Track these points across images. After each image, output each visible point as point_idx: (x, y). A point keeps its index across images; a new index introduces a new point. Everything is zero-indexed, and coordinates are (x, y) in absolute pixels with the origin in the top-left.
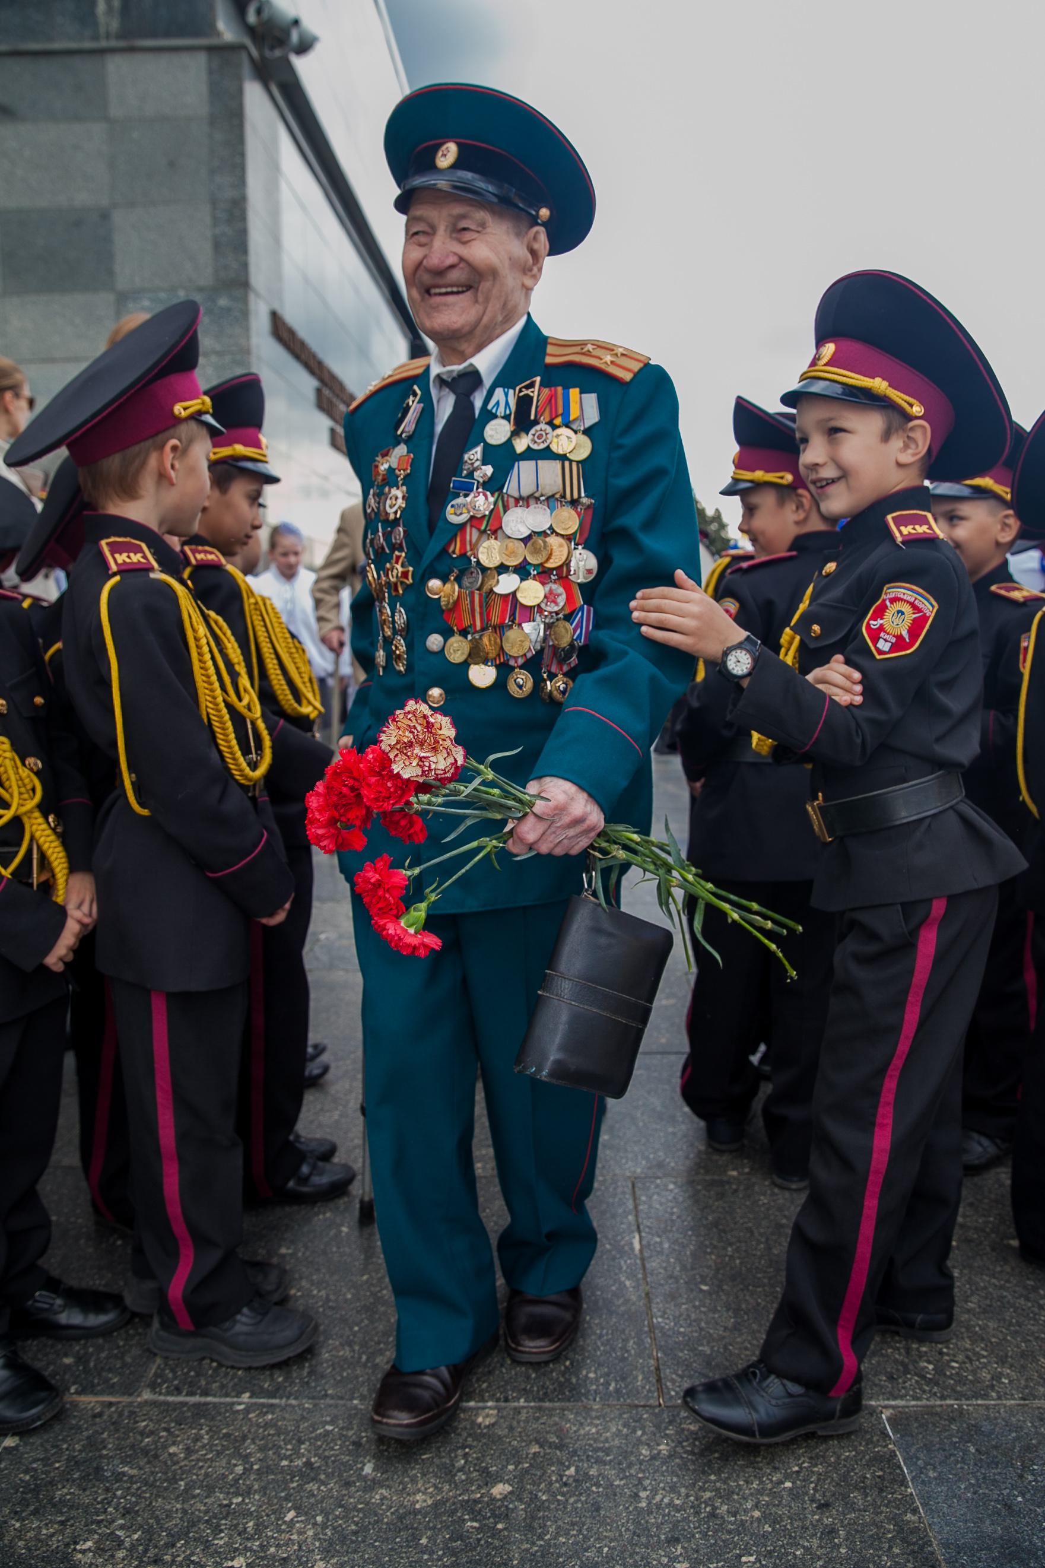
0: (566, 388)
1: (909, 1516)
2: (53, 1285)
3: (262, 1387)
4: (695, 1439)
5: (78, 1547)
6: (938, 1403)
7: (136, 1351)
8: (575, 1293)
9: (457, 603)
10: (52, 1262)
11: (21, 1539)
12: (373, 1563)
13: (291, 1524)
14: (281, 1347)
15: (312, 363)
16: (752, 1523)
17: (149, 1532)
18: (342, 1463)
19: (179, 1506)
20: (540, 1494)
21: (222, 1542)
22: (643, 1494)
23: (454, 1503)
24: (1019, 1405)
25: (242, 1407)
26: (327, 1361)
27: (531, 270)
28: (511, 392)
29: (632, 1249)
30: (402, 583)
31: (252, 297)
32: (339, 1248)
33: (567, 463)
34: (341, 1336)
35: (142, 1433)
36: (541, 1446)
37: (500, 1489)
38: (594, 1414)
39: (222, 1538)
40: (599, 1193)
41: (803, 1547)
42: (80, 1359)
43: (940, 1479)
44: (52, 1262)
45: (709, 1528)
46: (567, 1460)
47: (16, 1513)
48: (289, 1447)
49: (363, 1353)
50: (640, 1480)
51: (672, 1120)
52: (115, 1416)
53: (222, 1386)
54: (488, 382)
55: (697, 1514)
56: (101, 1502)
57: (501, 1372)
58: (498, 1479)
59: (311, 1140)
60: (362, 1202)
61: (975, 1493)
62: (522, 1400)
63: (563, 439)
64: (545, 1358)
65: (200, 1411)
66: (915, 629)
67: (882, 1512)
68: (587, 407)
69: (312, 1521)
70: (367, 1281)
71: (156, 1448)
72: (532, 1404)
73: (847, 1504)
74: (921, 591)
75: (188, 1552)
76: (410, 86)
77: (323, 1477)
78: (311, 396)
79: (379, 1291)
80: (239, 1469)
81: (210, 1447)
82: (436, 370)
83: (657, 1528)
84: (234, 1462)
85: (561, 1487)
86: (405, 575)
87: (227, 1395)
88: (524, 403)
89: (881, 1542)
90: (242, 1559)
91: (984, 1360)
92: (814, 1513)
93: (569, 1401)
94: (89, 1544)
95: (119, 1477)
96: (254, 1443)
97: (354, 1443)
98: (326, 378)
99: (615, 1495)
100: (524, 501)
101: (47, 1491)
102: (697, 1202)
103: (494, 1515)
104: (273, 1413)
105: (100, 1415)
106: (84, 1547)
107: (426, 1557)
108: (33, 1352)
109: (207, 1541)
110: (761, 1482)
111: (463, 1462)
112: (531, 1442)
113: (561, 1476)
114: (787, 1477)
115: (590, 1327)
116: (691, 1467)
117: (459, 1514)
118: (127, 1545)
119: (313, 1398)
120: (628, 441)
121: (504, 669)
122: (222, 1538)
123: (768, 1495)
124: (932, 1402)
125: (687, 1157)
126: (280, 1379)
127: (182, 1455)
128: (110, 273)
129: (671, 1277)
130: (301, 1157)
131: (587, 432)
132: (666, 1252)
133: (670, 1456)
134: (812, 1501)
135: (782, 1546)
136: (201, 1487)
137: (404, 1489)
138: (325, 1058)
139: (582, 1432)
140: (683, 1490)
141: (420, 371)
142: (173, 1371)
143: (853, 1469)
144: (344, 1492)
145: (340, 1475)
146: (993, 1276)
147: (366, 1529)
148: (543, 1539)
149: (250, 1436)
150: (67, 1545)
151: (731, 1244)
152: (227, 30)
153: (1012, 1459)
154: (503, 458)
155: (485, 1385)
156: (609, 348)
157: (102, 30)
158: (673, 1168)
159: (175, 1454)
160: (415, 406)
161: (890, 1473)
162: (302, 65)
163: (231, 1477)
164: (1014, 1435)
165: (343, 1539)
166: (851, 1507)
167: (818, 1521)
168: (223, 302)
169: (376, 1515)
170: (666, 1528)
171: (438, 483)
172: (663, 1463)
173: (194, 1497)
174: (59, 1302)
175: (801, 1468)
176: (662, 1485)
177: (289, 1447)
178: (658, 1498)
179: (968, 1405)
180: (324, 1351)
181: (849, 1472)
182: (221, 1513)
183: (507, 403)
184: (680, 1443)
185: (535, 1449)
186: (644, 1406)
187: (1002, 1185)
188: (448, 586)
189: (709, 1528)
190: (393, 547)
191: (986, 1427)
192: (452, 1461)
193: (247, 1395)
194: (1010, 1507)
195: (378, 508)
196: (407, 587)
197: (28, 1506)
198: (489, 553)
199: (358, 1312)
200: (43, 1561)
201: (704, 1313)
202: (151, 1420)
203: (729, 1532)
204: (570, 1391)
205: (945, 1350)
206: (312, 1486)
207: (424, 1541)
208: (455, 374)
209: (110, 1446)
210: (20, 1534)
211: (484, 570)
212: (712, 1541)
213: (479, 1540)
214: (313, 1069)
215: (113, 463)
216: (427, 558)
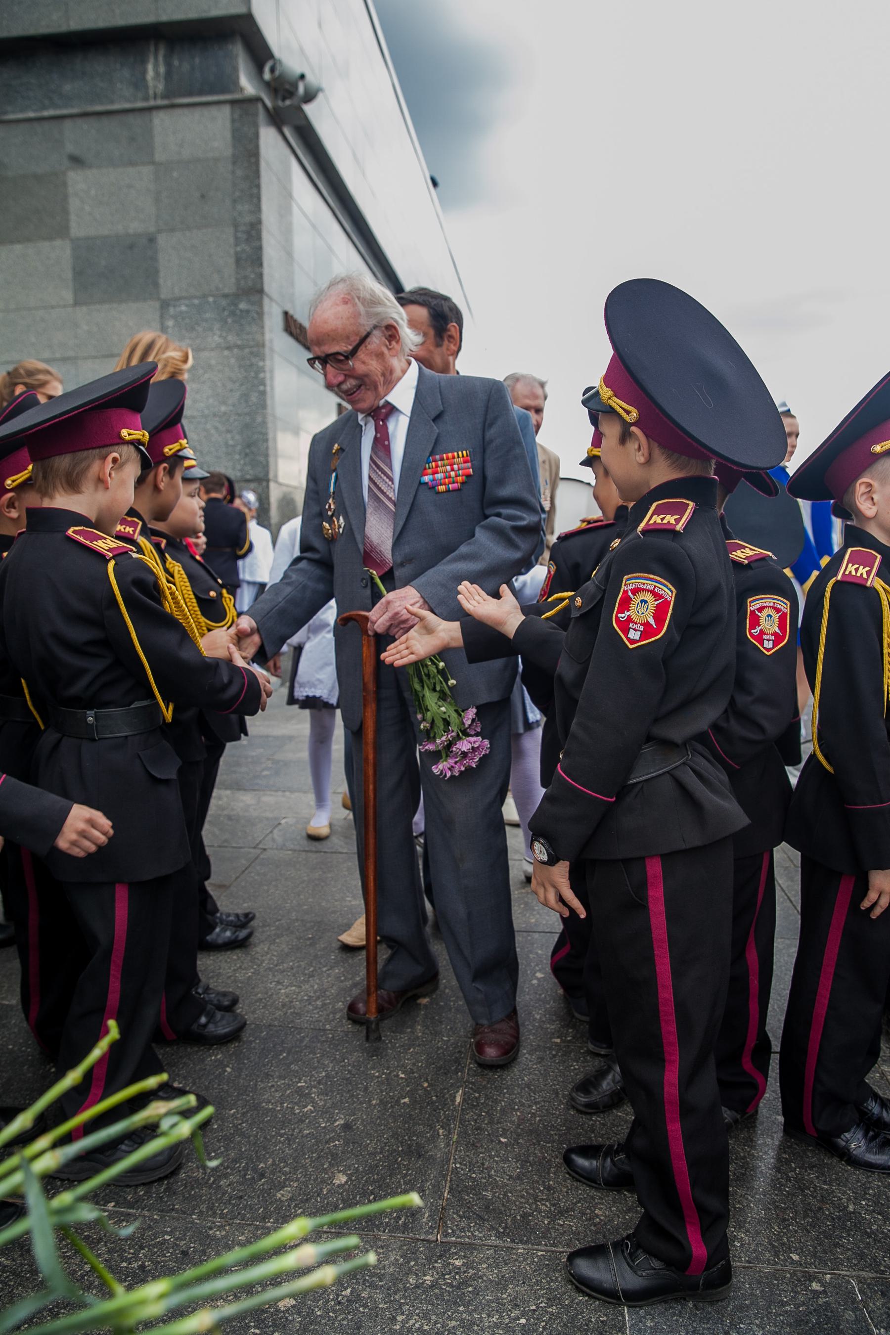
3: (125, 1199)
4: (457, 1273)
22: (400, 1318)
24: (744, 1267)
26: (182, 1180)
31: (266, 301)
46: (347, 1282)
48: (132, 1251)
49: (212, 1176)
50: (401, 1305)
57: (316, 1201)
66: (659, 614)
72: (333, 1230)
74: (658, 578)
79: (240, 1124)
85: (335, 1305)
99: (377, 1317)
110: (501, 1317)
113: (338, 1295)
119: (162, 1211)
123: (503, 1329)
126: (141, 1193)
128: (156, 284)
130: (201, 1007)
140: (434, 1317)
149: (104, 1240)
151: (536, 1103)
152: (248, 85)
153: (723, 1316)
157: (151, 92)
161: (613, 1319)
162: (309, 109)
168: (243, 306)
176: (417, 1311)
177: (132, 1251)
178: (411, 1322)
180: (183, 1171)
181: (577, 1315)
184: (444, 1275)
186: (423, 1240)
201: (497, 1162)
215: (63, 462)
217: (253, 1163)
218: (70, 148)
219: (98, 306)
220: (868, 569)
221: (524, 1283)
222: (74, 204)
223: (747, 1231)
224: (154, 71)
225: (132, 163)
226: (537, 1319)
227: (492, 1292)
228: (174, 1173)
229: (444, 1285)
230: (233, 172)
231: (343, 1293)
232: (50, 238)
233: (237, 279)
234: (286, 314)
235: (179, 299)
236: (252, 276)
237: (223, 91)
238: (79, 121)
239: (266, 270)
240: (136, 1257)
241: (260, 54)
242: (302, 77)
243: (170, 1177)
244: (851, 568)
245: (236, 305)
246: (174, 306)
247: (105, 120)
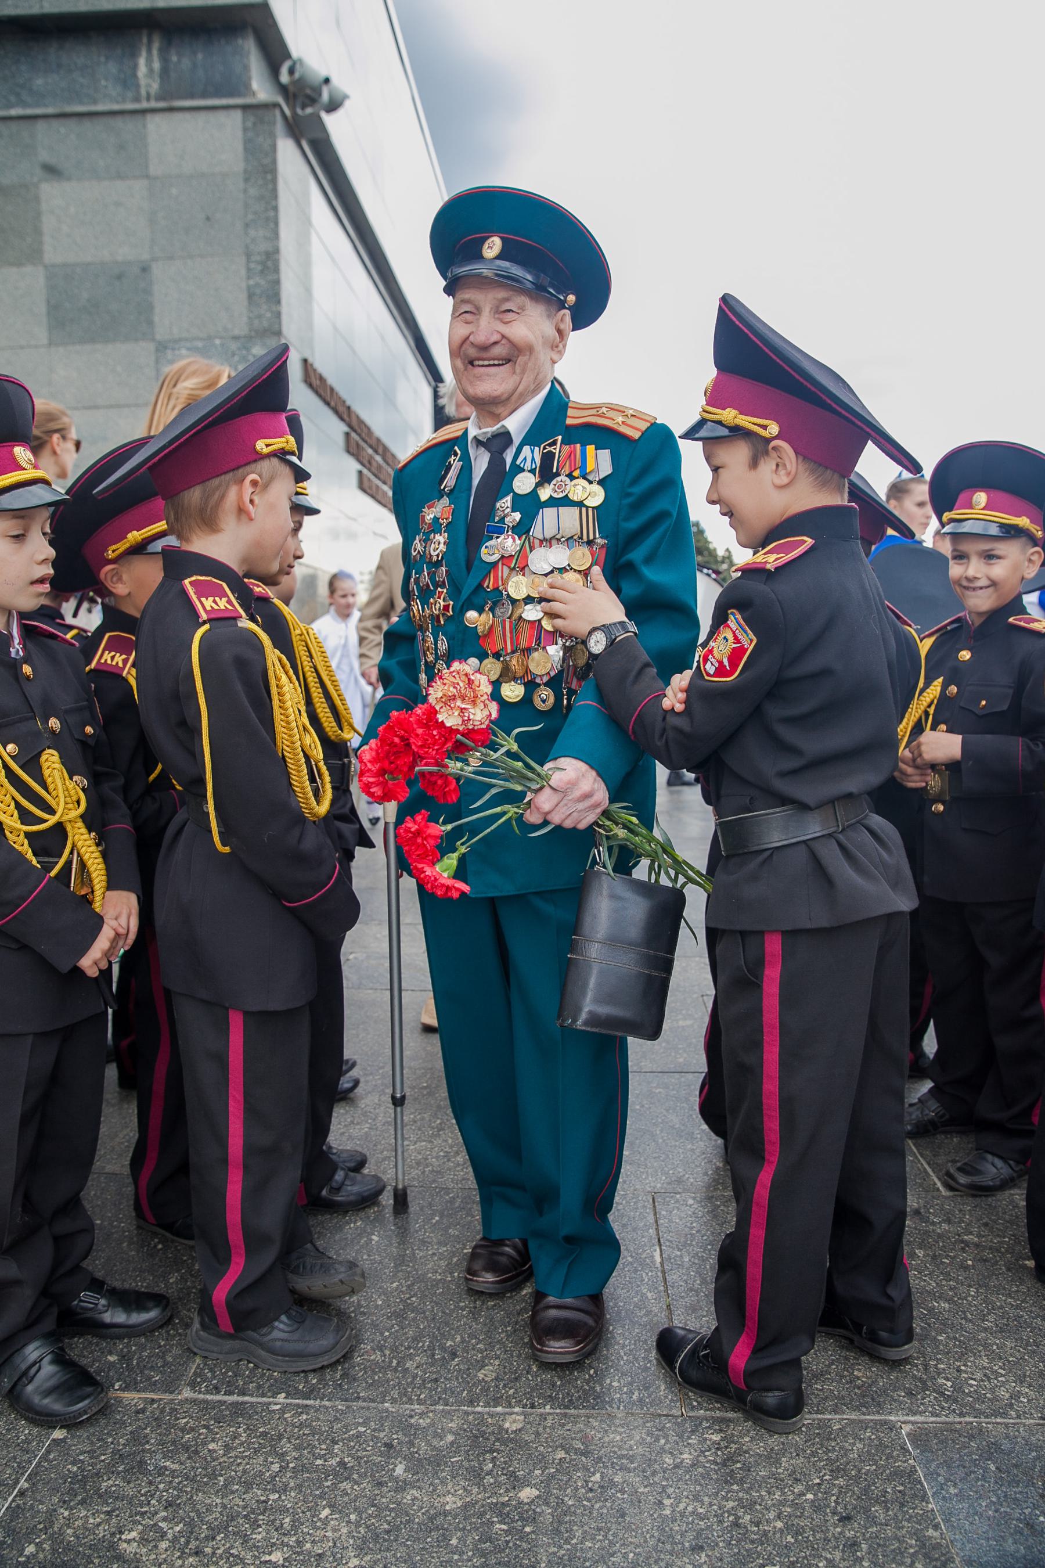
0: (584, 445)
1: (931, 1532)
2: (97, 1285)
3: (296, 1388)
4: (718, 1449)
5: (123, 1537)
6: (958, 1419)
7: (176, 1351)
8: (597, 1299)
9: (491, 628)
10: (96, 1265)
11: (69, 1527)
12: (405, 1562)
13: (326, 1521)
14: (315, 1355)
15: (341, 409)
16: (774, 1534)
17: (191, 1525)
18: (374, 1464)
19: (218, 1501)
20: (566, 1499)
21: (259, 1537)
23: (483, 1506)
25: (278, 1407)
26: (359, 1365)
27: (557, 347)
28: (537, 449)
29: (653, 1262)
30: (443, 615)
32: (369, 1256)
33: (584, 509)
34: (373, 1341)
35: (183, 1430)
36: (567, 1453)
37: (527, 1494)
38: (618, 1422)
39: (259, 1533)
40: (620, 1207)
41: (826, 1559)
42: (123, 1357)
43: (961, 1496)
44: (96, 1265)
45: (732, 1537)
47: (65, 1502)
48: (323, 1447)
51: (691, 1137)
52: (157, 1412)
53: (259, 1387)
54: (517, 441)
55: (721, 1522)
56: (145, 1495)
57: (528, 1379)
58: (525, 1483)
59: (342, 1151)
60: (396, 1189)
61: (996, 1511)
62: (548, 1407)
63: (580, 488)
64: (569, 1359)
65: (238, 1410)
67: (903, 1527)
68: (600, 461)
69: (346, 1519)
70: (397, 1288)
71: (196, 1444)
72: (558, 1411)
73: (868, 1517)
75: (228, 1545)
76: (448, 194)
77: (355, 1476)
78: (341, 440)
79: (409, 1298)
80: (276, 1467)
81: (248, 1444)
82: (473, 432)
83: (682, 1535)
84: (270, 1459)
85: (587, 1493)
86: (446, 608)
87: (263, 1395)
88: (548, 458)
89: (904, 1557)
90: (279, 1554)
91: (1003, 1379)
92: (836, 1526)
93: (594, 1409)
94: (134, 1534)
95: (161, 1471)
96: (290, 1442)
97: (386, 1445)
98: (354, 423)
100: (547, 542)
101: (94, 1482)
102: (715, 1217)
103: (522, 1519)
104: (307, 1414)
105: (143, 1411)
106: (130, 1537)
107: (456, 1557)
108: (80, 1349)
109: (246, 1535)
110: (783, 1493)
111: (491, 1465)
112: (557, 1447)
114: (809, 1489)
115: (614, 1338)
116: (714, 1477)
117: (488, 1517)
118: (170, 1536)
119: (346, 1400)
120: (637, 490)
121: (531, 686)
122: (259, 1533)
123: (790, 1506)
124: (950, 1419)
125: (706, 1174)
126: (314, 1381)
127: (221, 1452)
128: (150, 323)
129: (691, 1290)
131: (601, 482)
132: (687, 1265)
133: (693, 1465)
134: (834, 1513)
135: (805, 1557)
136: (239, 1483)
137: (434, 1491)
138: (354, 1073)
139: (606, 1439)
140: (706, 1499)
141: (460, 433)
142: (211, 1370)
143: (874, 1484)
144: (376, 1492)
145: (373, 1476)
146: (1009, 1295)
147: (398, 1529)
148: (569, 1543)
149: (286, 1435)
150: (113, 1534)
152: (261, 89)
154: (529, 505)
155: (511, 1392)
156: (620, 410)
157: (143, 92)
158: (692, 1184)
159: (214, 1451)
160: (456, 465)
161: (911, 1489)
163: (267, 1474)
164: (1034, 1454)
165: (376, 1538)
166: (873, 1520)
167: (840, 1533)
169: (407, 1515)
170: (690, 1536)
171: (476, 526)
172: (687, 1472)
173: (233, 1492)
174: (103, 1302)
175: (822, 1480)
176: (685, 1493)
177: (323, 1447)
178: (682, 1506)
179: (987, 1423)
181: (869, 1486)
182: (259, 1508)
183: (533, 459)
184: (703, 1452)
185: (561, 1454)
187: (1017, 1206)
188: (484, 616)
189: (732, 1537)
190: (437, 585)
191: (1006, 1445)
192: (480, 1464)
193: (283, 1395)
194: (1032, 1527)
195: (424, 552)
196: (448, 619)
197: (76, 1495)
198: (518, 587)
199: (388, 1318)
200: (90, 1549)
202: (192, 1417)
203: (753, 1542)
204: (594, 1400)
205: (963, 1368)
206: (346, 1485)
207: (454, 1542)
208: (489, 435)
209: (153, 1441)
210: (69, 1522)
211: (514, 602)
212: (736, 1550)
213: (507, 1542)
214: (345, 1083)
216: (466, 593)
217: (438, 1341)
218: (44, 156)
219: (78, 347)
220: (124, 657)
221: (798, 1455)
222: (48, 223)
223: (1030, 1385)
224: (146, 65)
225: (120, 176)
226: (825, 1493)
227: (764, 1467)
228: (346, 1357)
229: (707, 1462)
230: (245, 191)
231: (592, 1479)
232: (19, 264)
233: (250, 318)
234: (305, 361)
235: (180, 340)
236: (269, 315)
237: (232, 94)
238: (55, 123)
239: (285, 309)
240: (330, 1452)
241: (275, 52)
242: (327, 81)
243: (344, 1362)
244: (107, 656)
245: (248, 349)
246: (173, 349)
247: (87, 123)
